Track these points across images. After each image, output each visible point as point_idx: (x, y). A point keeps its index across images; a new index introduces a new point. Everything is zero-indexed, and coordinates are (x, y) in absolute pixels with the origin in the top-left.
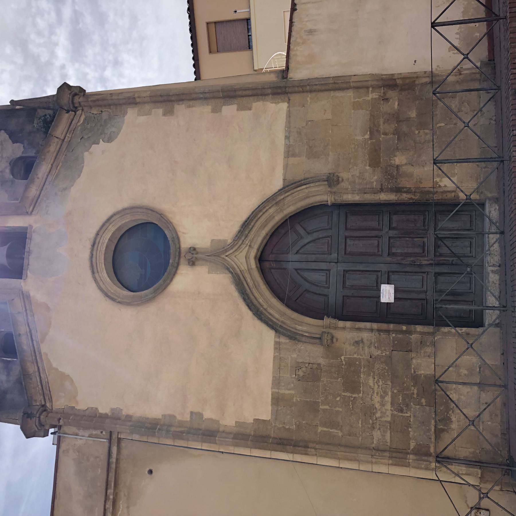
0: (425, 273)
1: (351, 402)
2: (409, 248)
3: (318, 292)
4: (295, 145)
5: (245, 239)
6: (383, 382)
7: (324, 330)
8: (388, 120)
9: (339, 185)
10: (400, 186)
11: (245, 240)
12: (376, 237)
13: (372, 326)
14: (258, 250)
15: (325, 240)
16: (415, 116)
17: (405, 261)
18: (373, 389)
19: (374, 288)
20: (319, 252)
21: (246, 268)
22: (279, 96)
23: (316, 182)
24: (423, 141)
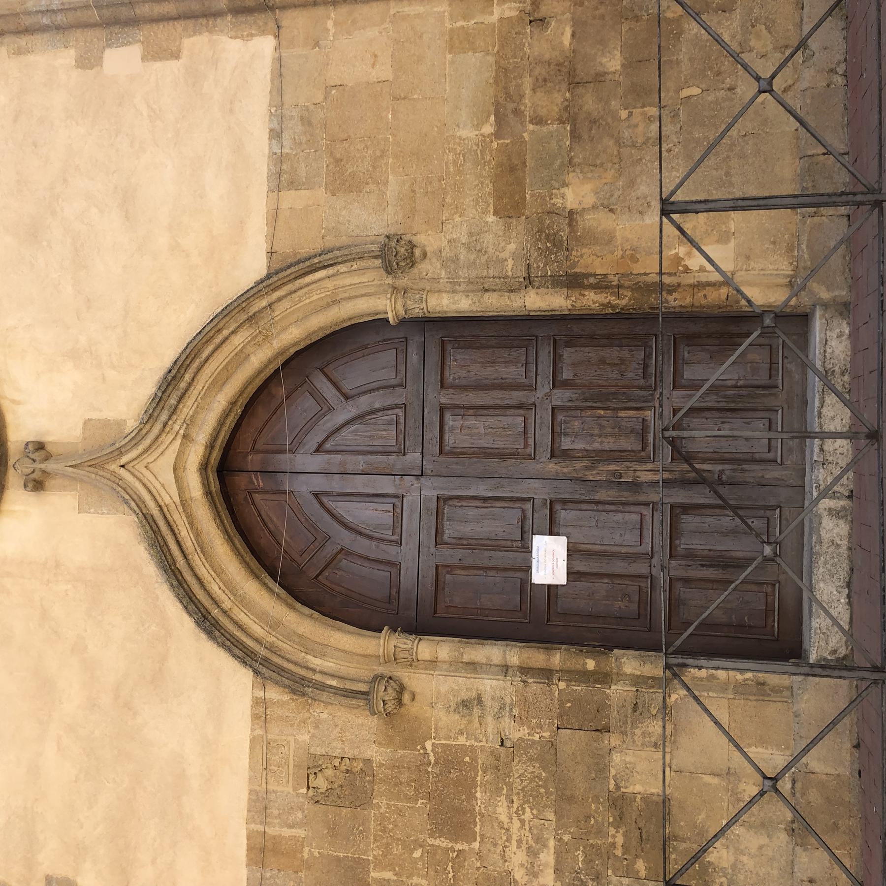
0: (647, 504)
1: (450, 864)
2: (606, 436)
3: (373, 555)
4: (296, 154)
5: (170, 418)
6: (535, 812)
7: (380, 670)
8: (545, 80)
9: (415, 270)
10: (577, 270)
11: (170, 422)
12: (519, 407)
13: (504, 657)
14: (210, 447)
15: (391, 416)
16: (619, 67)
17: (594, 472)
18: (507, 830)
19: (515, 544)
20: (375, 449)
21: (177, 499)
22: (251, 19)
23: (354, 260)
24: (640, 140)
